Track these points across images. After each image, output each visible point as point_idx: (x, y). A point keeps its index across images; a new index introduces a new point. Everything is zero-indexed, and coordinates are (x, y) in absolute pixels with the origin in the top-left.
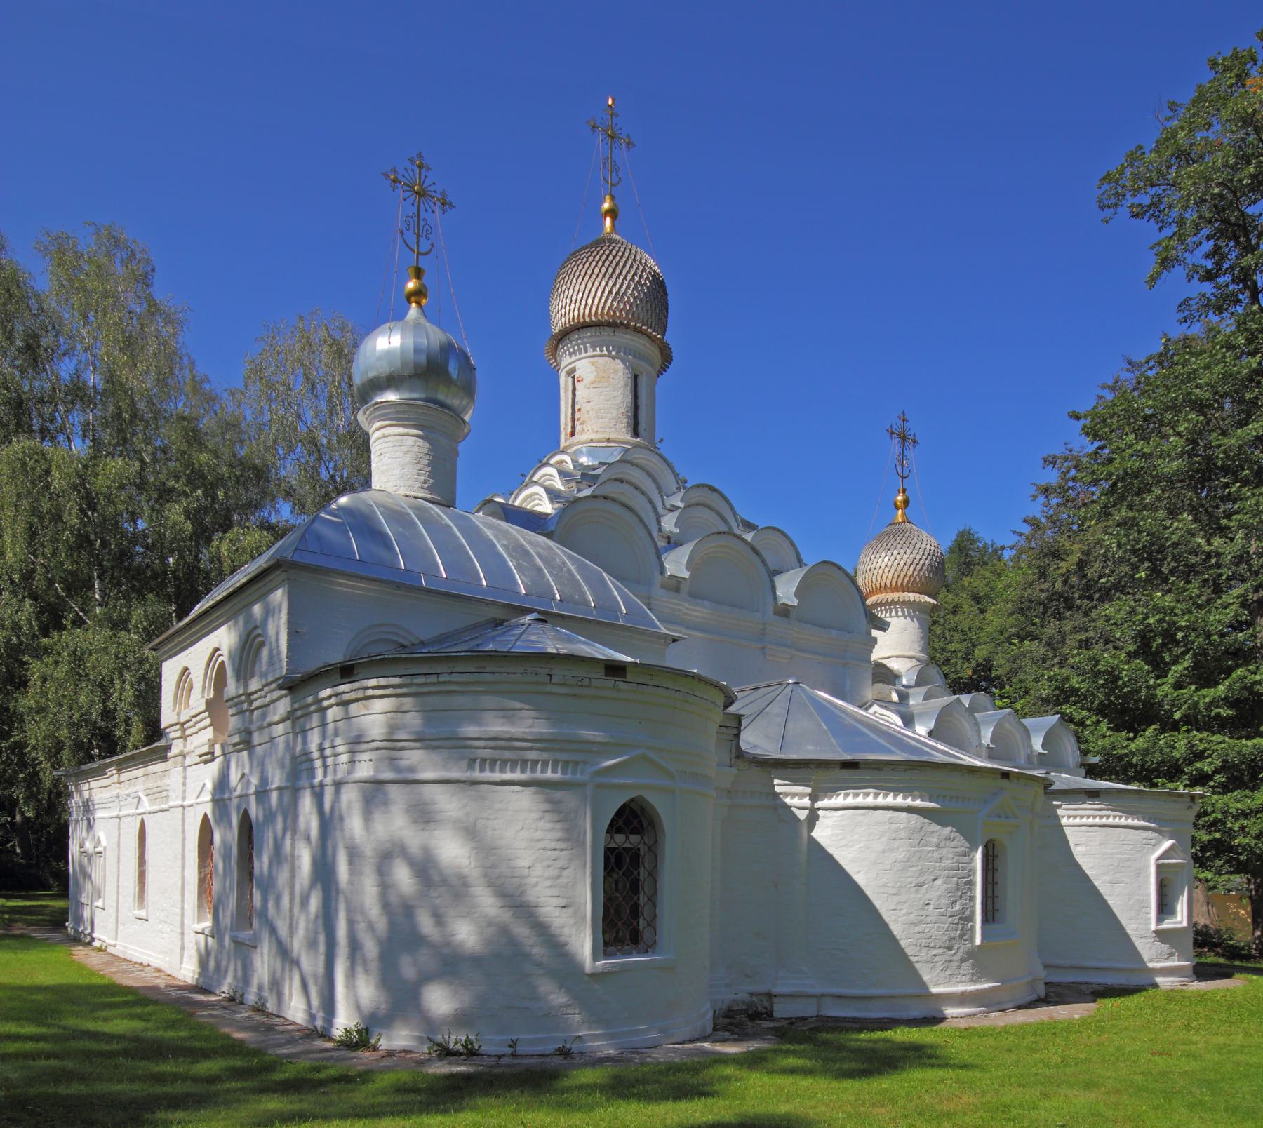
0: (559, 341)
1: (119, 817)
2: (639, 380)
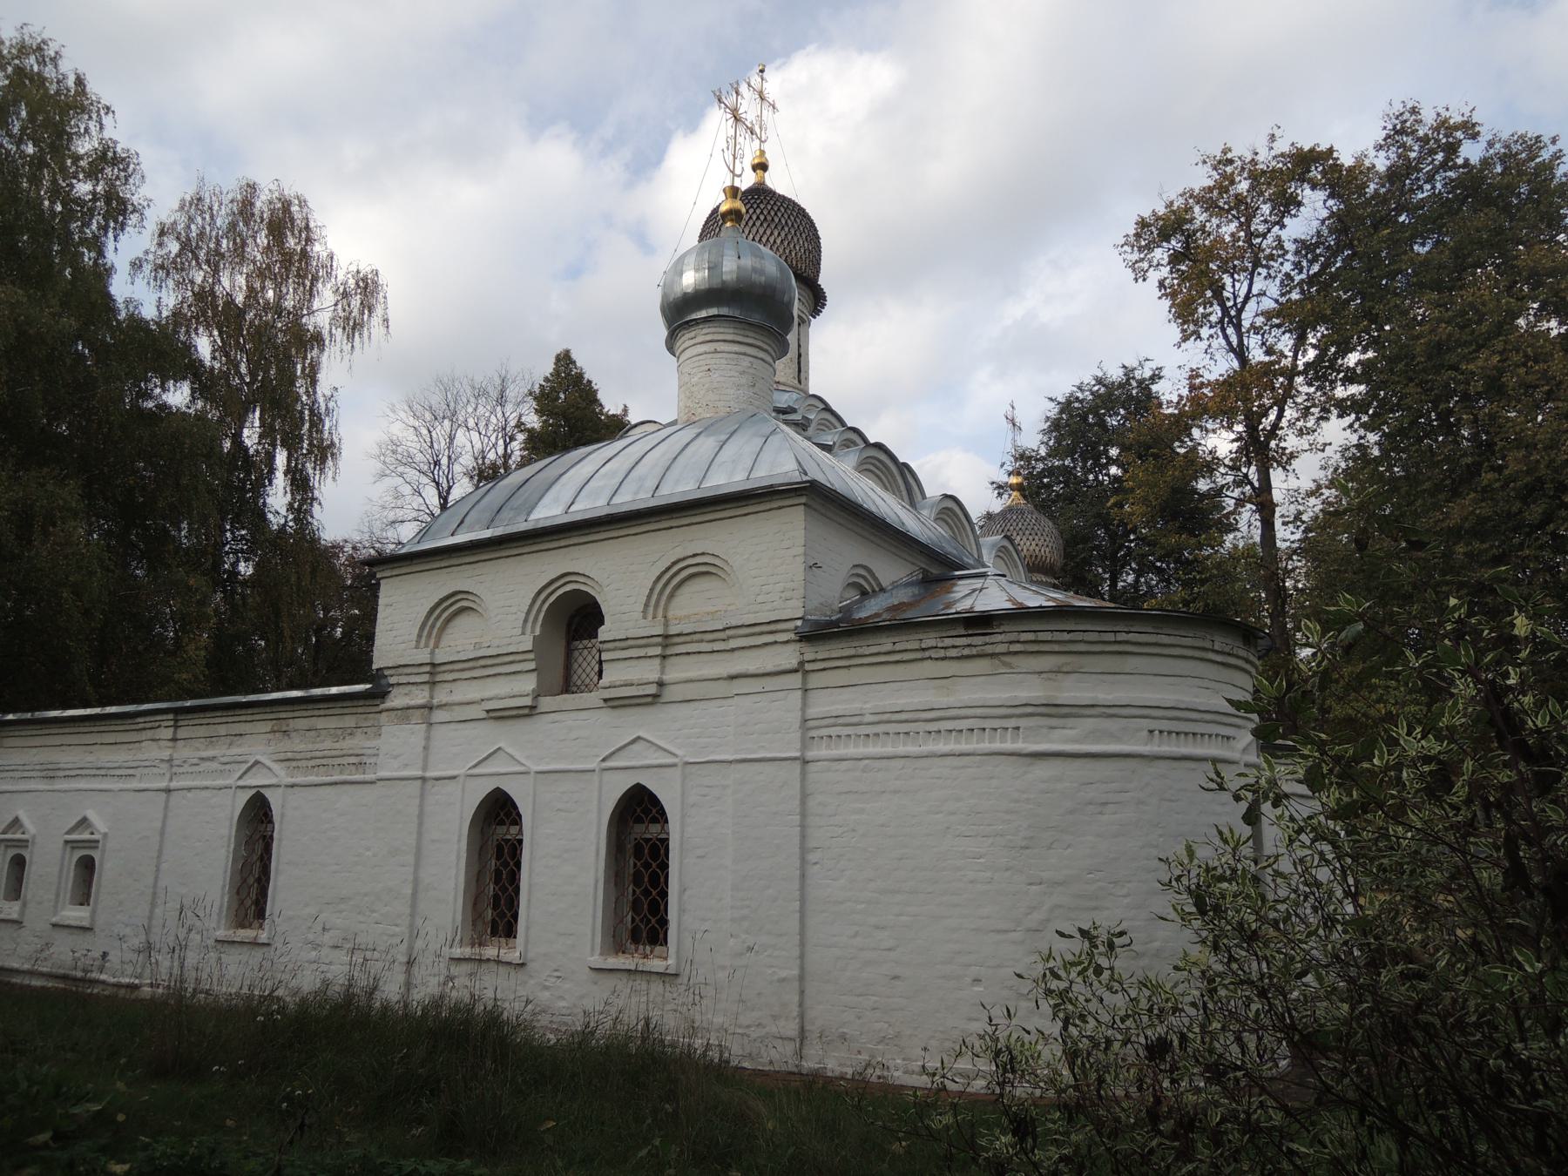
1: (168, 791)
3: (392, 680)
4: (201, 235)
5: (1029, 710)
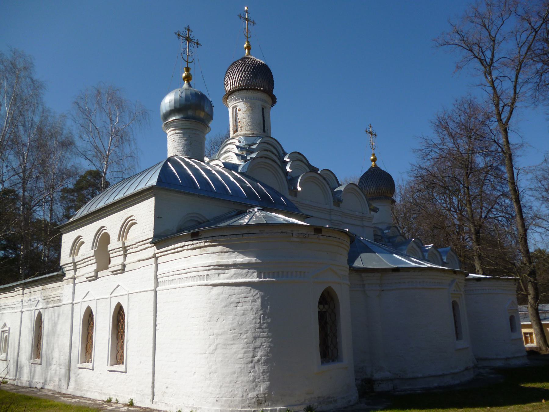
0: (229, 95)
2: (265, 110)
3: (66, 269)
4: (461, 163)
5: (211, 267)
